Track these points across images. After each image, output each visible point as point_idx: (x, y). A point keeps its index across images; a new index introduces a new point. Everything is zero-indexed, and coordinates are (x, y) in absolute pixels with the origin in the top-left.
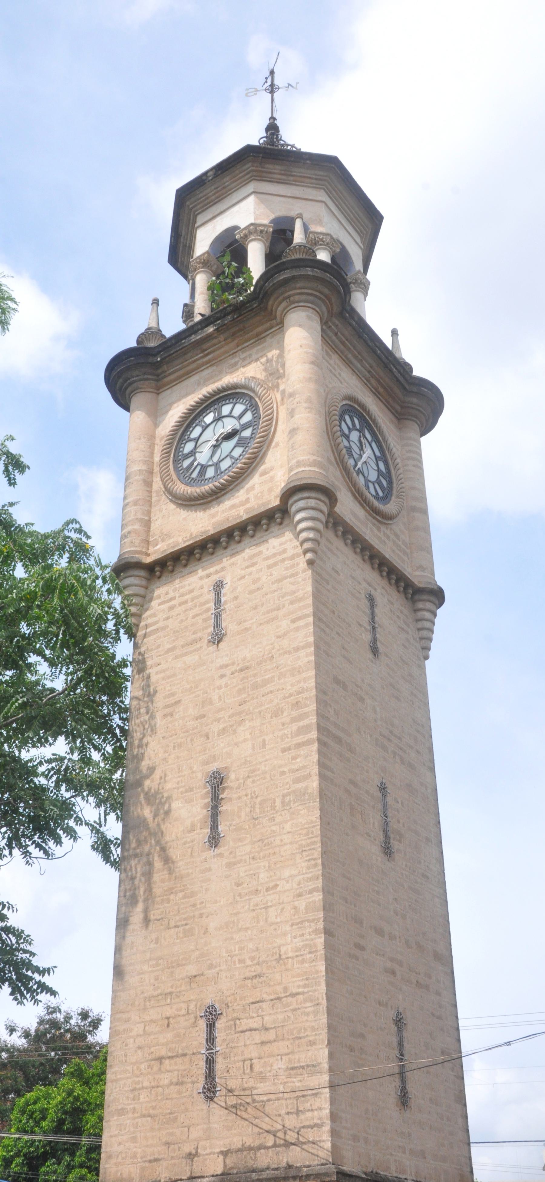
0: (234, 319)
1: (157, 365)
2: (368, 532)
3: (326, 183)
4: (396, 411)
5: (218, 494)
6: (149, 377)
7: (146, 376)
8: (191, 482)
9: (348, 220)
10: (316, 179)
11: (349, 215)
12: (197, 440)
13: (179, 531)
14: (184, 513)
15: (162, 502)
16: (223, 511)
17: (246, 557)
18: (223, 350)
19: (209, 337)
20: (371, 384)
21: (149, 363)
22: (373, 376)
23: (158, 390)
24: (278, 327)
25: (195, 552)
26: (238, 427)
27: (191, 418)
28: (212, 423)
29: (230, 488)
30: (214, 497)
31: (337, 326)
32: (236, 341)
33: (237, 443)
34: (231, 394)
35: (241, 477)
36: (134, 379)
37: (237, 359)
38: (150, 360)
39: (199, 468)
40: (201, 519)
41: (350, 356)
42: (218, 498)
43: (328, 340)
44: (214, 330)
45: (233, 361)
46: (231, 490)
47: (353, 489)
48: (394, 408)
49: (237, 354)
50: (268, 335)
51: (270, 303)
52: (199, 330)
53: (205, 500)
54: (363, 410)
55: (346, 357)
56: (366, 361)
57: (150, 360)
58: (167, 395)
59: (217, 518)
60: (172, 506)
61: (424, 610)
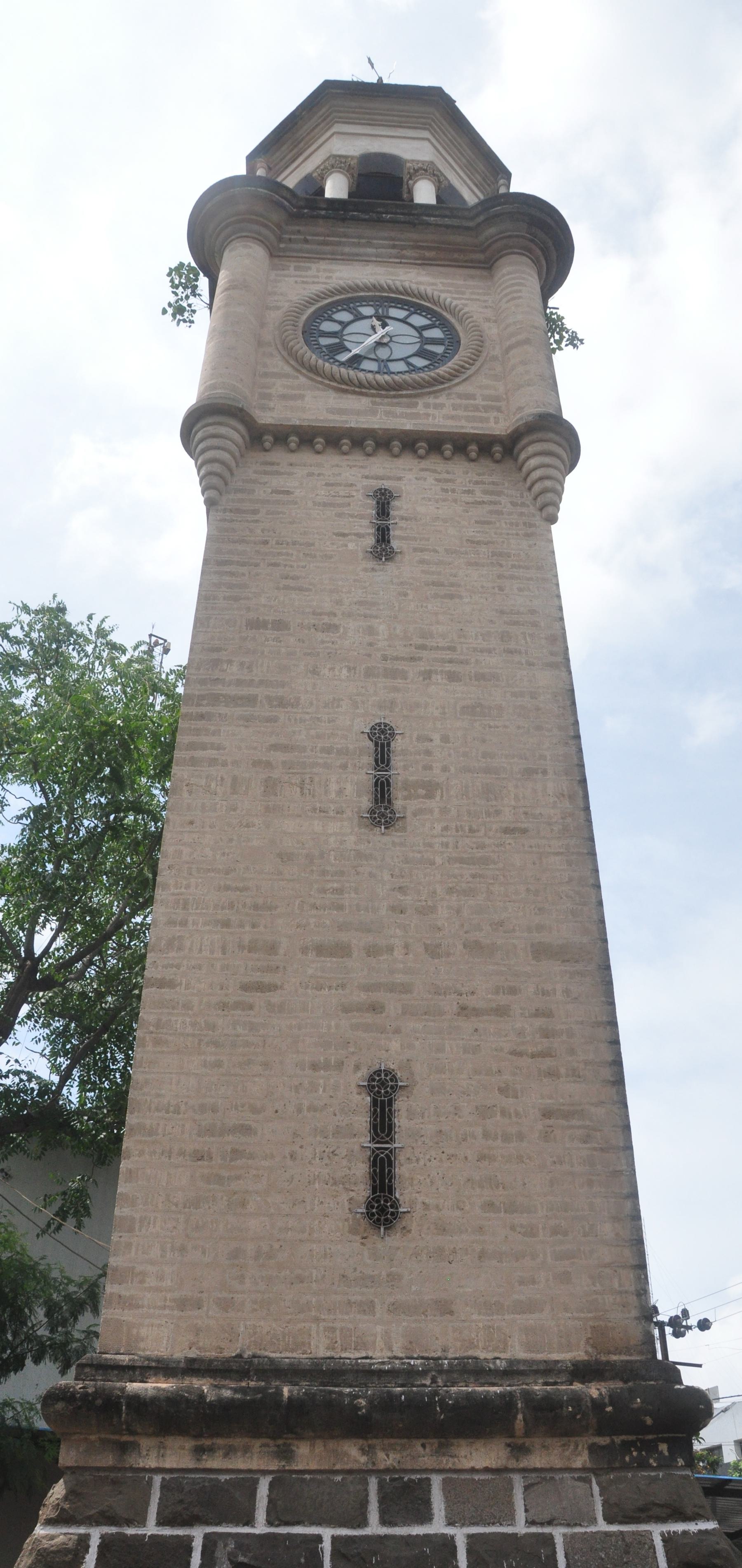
2: (463, 423)
3: (335, 114)
4: (480, 262)
9: (394, 126)
10: (323, 121)
11: (393, 121)
12: (344, 325)
20: (410, 258)
22: (403, 248)
31: (299, 232)
41: (347, 250)
43: (442, 263)
47: (335, 384)
48: (472, 261)
54: (379, 291)
55: (342, 254)
56: (375, 238)
61: (528, 458)
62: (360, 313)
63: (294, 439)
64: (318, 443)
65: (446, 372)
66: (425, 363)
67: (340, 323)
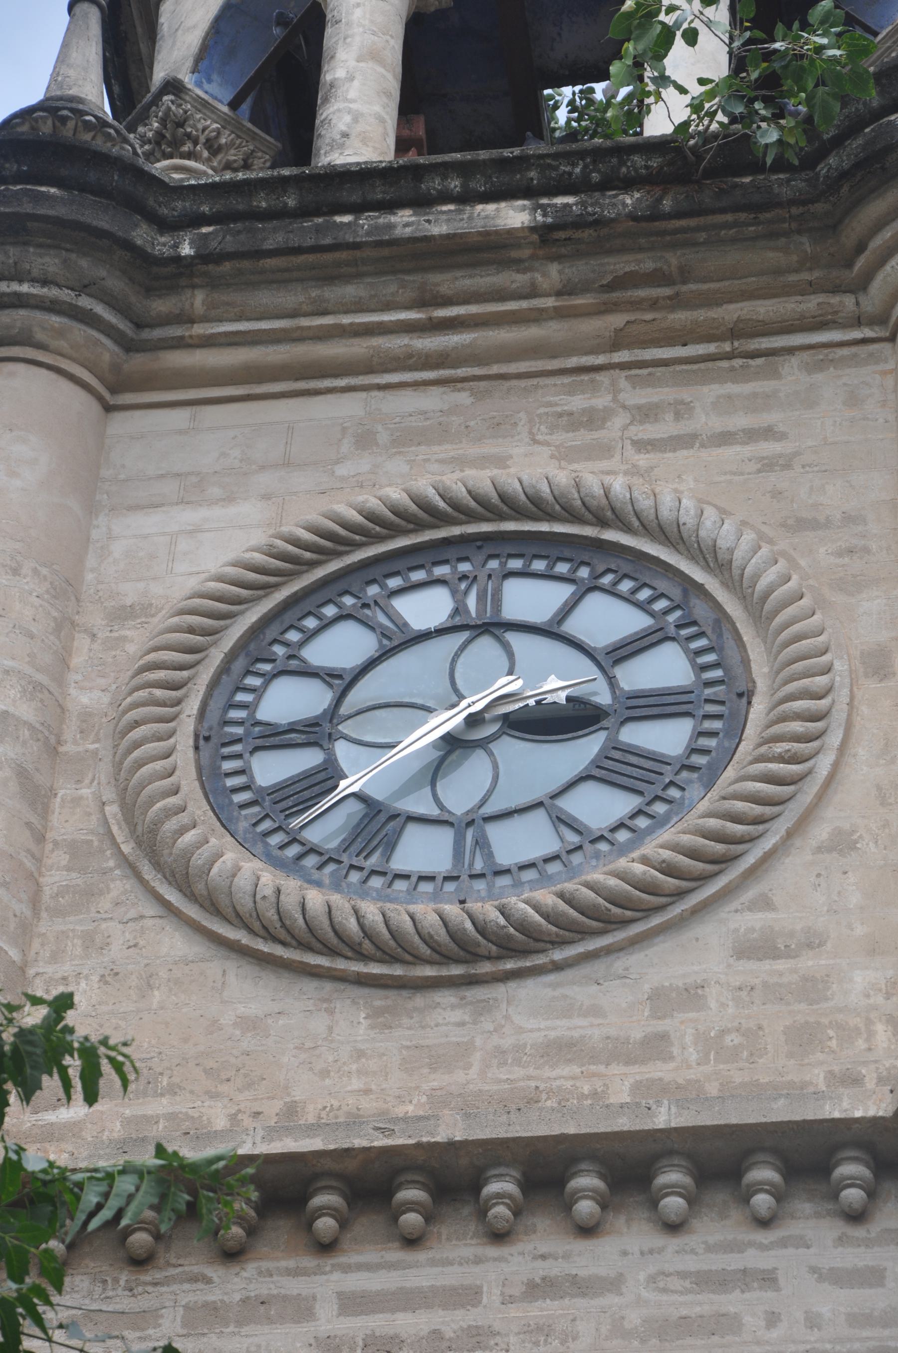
0: (655, 216)
1: (173, 274)
5: (483, 956)
6: (100, 309)
7: (85, 302)
8: (302, 857)
12: (343, 681)
13: (208, 1072)
14: (248, 994)
15: (105, 904)
16: (500, 1052)
17: (633, 1318)
18: (532, 332)
19: (492, 248)
21: (128, 245)
23: (115, 391)
24: (857, 334)
25: (319, 1200)
26: (603, 697)
27: (320, 573)
28: (441, 632)
29: (558, 955)
30: (456, 970)
32: (617, 320)
33: (596, 764)
34: (577, 539)
35: (625, 923)
36: (25, 288)
37: (602, 401)
38: (141, 234)
39: (354, 807)
40: (360, 1054)
42: (472, 981)
44: (533, 229)
45: (578, 402)
46: (557, 967)
49: (603, 378)
50: (791, 351)
51: (876, 208)
52: (446, 197)
53: (398, 971)
57: (141, 234)
58: (154, 435)
59: (460, 1076)
60: (174, 944)
62: (403, 626)
63: (502, 1186)
64: (321, 1211)
65: (676, 848)
66: (620, 804)
67: (327, 676)
